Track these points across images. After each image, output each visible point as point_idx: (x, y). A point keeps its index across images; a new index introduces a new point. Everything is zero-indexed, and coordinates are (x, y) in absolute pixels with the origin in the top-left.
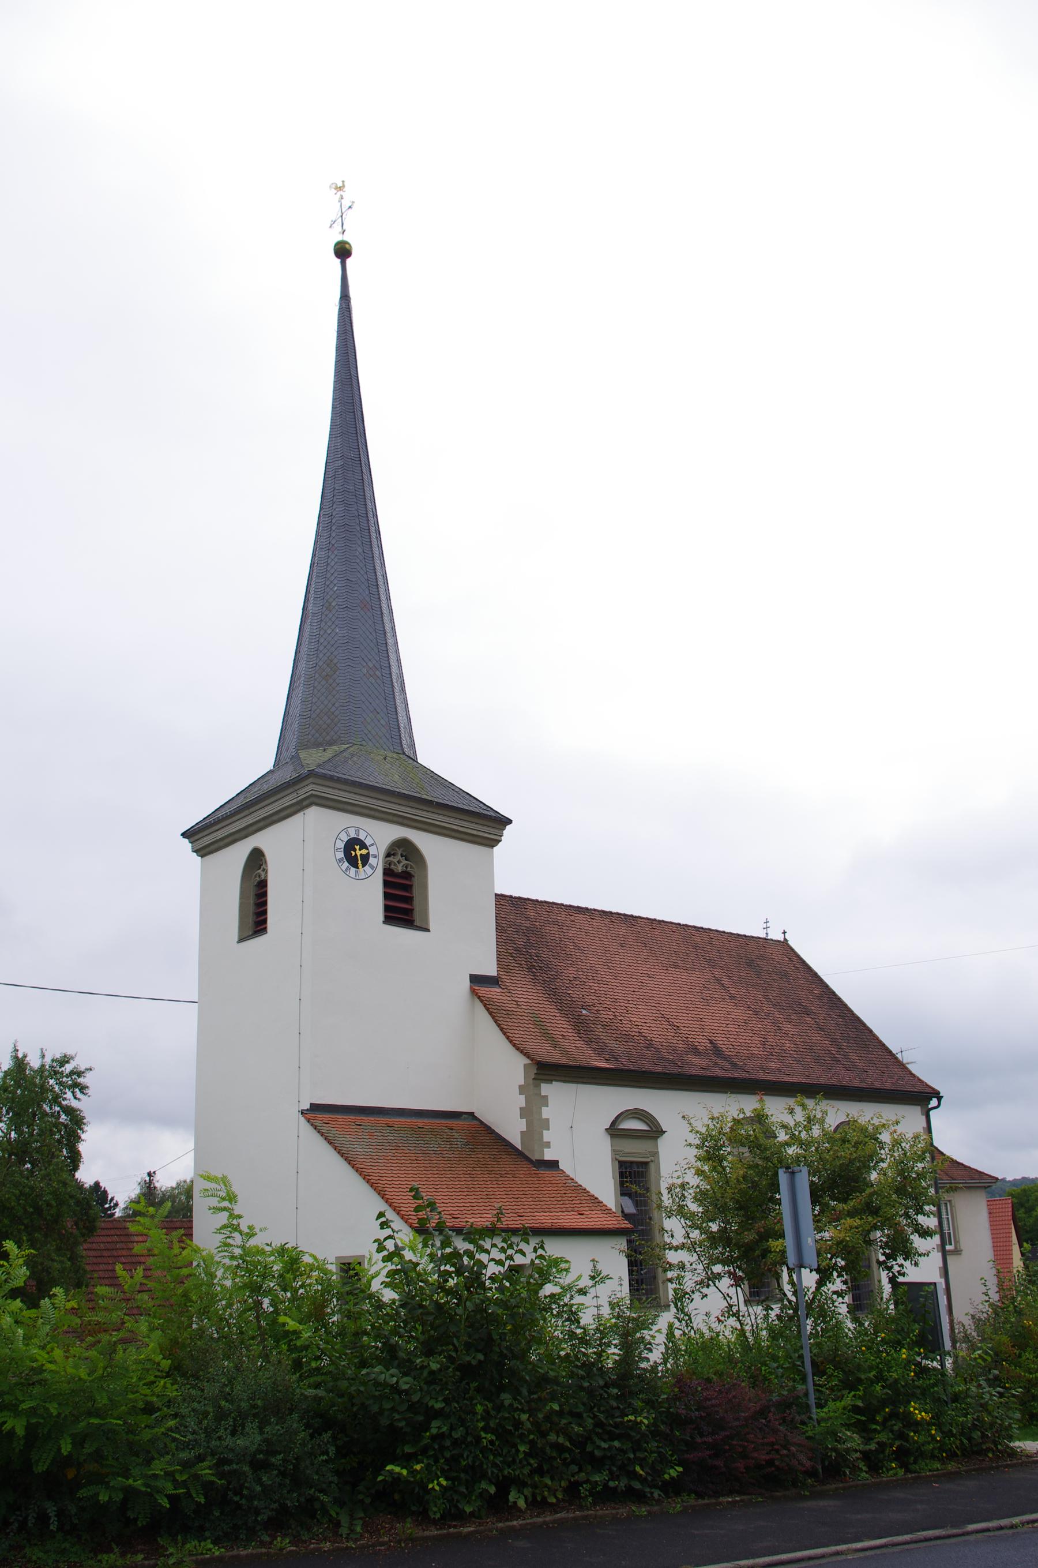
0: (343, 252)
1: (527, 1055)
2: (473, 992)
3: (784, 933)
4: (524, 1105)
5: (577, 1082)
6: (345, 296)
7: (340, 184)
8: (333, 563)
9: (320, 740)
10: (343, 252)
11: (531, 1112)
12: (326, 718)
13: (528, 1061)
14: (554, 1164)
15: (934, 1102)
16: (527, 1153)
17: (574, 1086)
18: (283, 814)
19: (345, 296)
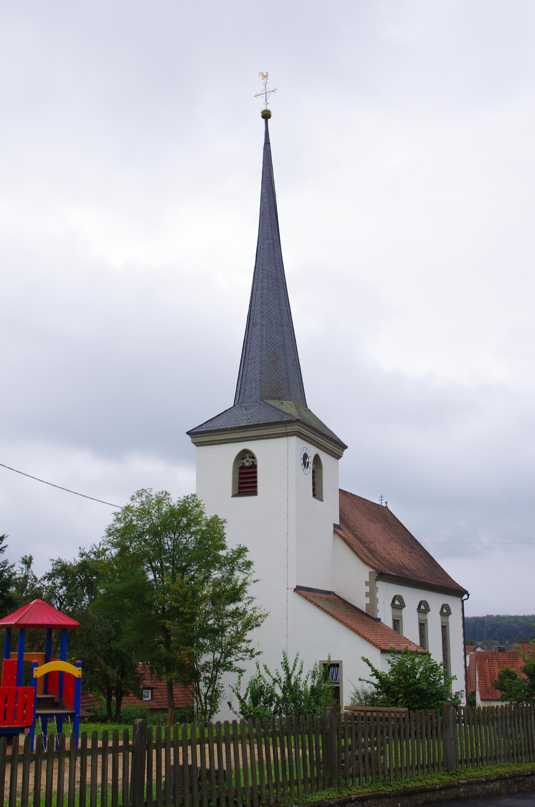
0: (266, 115)
1: (370, 566)
2: (335, 532)
3: (386, 503)
4: (368, 591)
5: (389, 582)
6: (267, 143)
7: (265, 74)
8: (271, 299)
9: (274, 396)
10: (266, 115)
11: (372, 594)
12: (275, 384)
13: (372, 570)
14: (379, 620)
15: (465, 596)
16: (369, 614)
17: (386, 584)
18: (271, 436)
19: (267, 143)
